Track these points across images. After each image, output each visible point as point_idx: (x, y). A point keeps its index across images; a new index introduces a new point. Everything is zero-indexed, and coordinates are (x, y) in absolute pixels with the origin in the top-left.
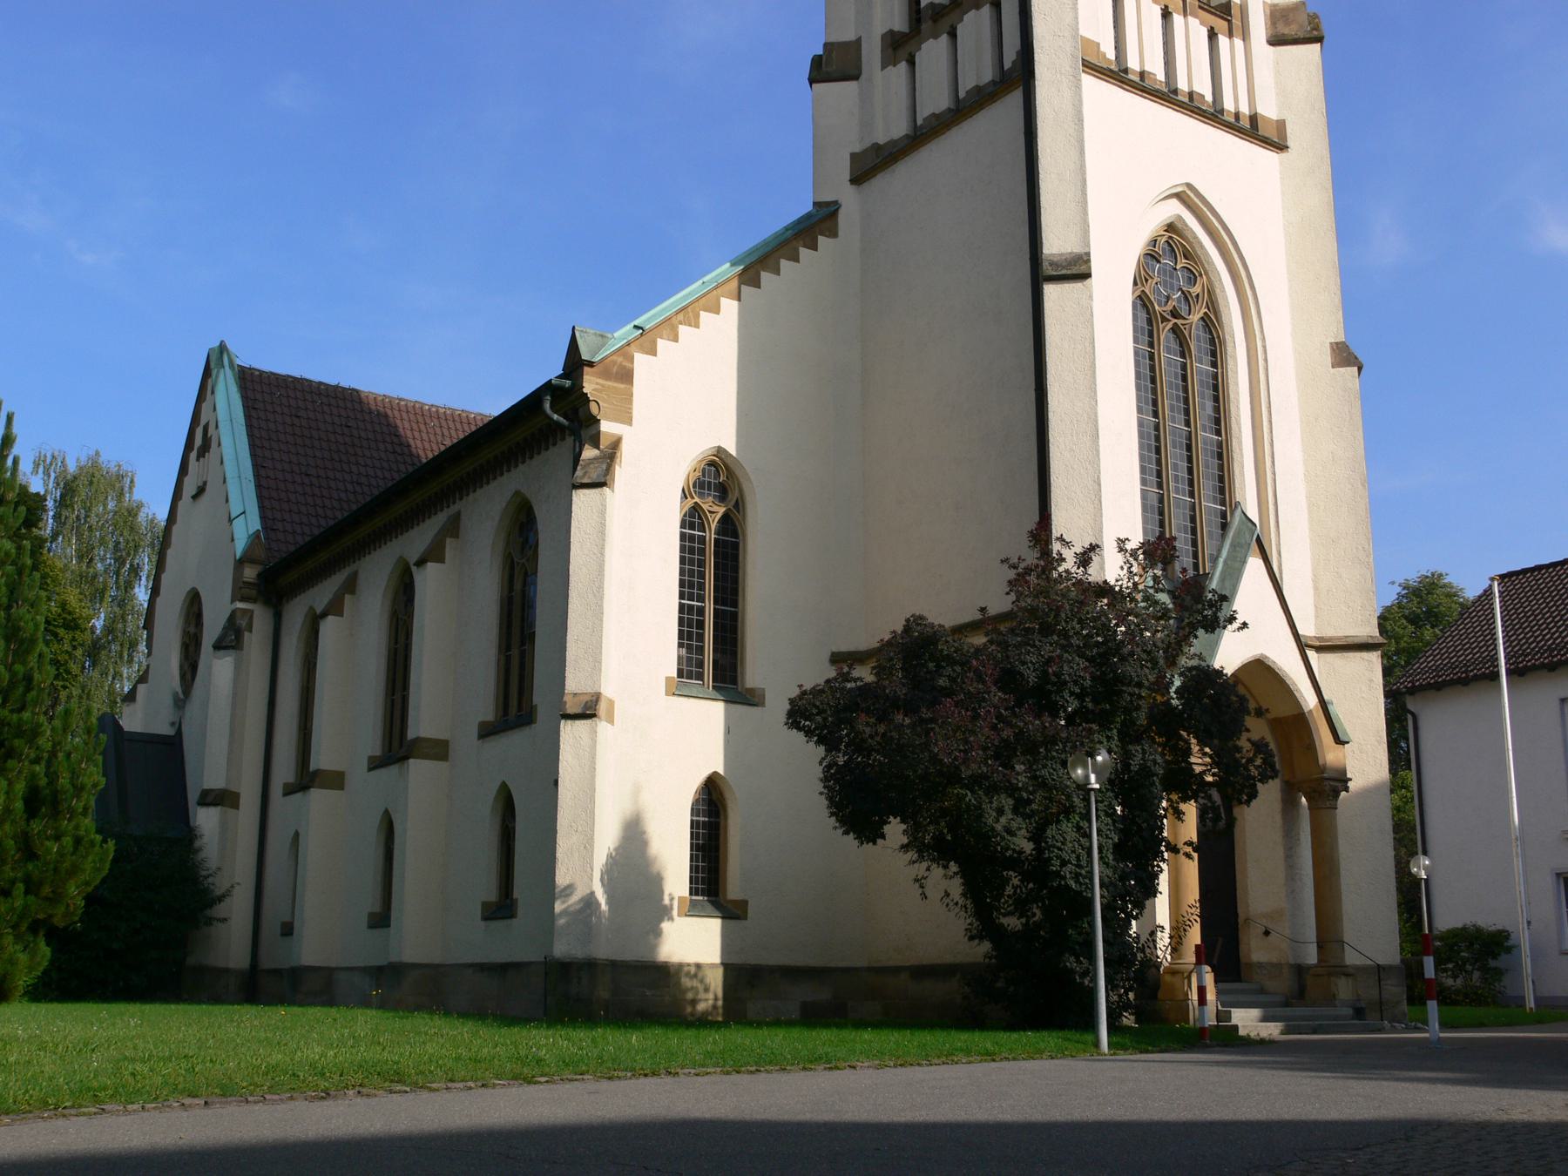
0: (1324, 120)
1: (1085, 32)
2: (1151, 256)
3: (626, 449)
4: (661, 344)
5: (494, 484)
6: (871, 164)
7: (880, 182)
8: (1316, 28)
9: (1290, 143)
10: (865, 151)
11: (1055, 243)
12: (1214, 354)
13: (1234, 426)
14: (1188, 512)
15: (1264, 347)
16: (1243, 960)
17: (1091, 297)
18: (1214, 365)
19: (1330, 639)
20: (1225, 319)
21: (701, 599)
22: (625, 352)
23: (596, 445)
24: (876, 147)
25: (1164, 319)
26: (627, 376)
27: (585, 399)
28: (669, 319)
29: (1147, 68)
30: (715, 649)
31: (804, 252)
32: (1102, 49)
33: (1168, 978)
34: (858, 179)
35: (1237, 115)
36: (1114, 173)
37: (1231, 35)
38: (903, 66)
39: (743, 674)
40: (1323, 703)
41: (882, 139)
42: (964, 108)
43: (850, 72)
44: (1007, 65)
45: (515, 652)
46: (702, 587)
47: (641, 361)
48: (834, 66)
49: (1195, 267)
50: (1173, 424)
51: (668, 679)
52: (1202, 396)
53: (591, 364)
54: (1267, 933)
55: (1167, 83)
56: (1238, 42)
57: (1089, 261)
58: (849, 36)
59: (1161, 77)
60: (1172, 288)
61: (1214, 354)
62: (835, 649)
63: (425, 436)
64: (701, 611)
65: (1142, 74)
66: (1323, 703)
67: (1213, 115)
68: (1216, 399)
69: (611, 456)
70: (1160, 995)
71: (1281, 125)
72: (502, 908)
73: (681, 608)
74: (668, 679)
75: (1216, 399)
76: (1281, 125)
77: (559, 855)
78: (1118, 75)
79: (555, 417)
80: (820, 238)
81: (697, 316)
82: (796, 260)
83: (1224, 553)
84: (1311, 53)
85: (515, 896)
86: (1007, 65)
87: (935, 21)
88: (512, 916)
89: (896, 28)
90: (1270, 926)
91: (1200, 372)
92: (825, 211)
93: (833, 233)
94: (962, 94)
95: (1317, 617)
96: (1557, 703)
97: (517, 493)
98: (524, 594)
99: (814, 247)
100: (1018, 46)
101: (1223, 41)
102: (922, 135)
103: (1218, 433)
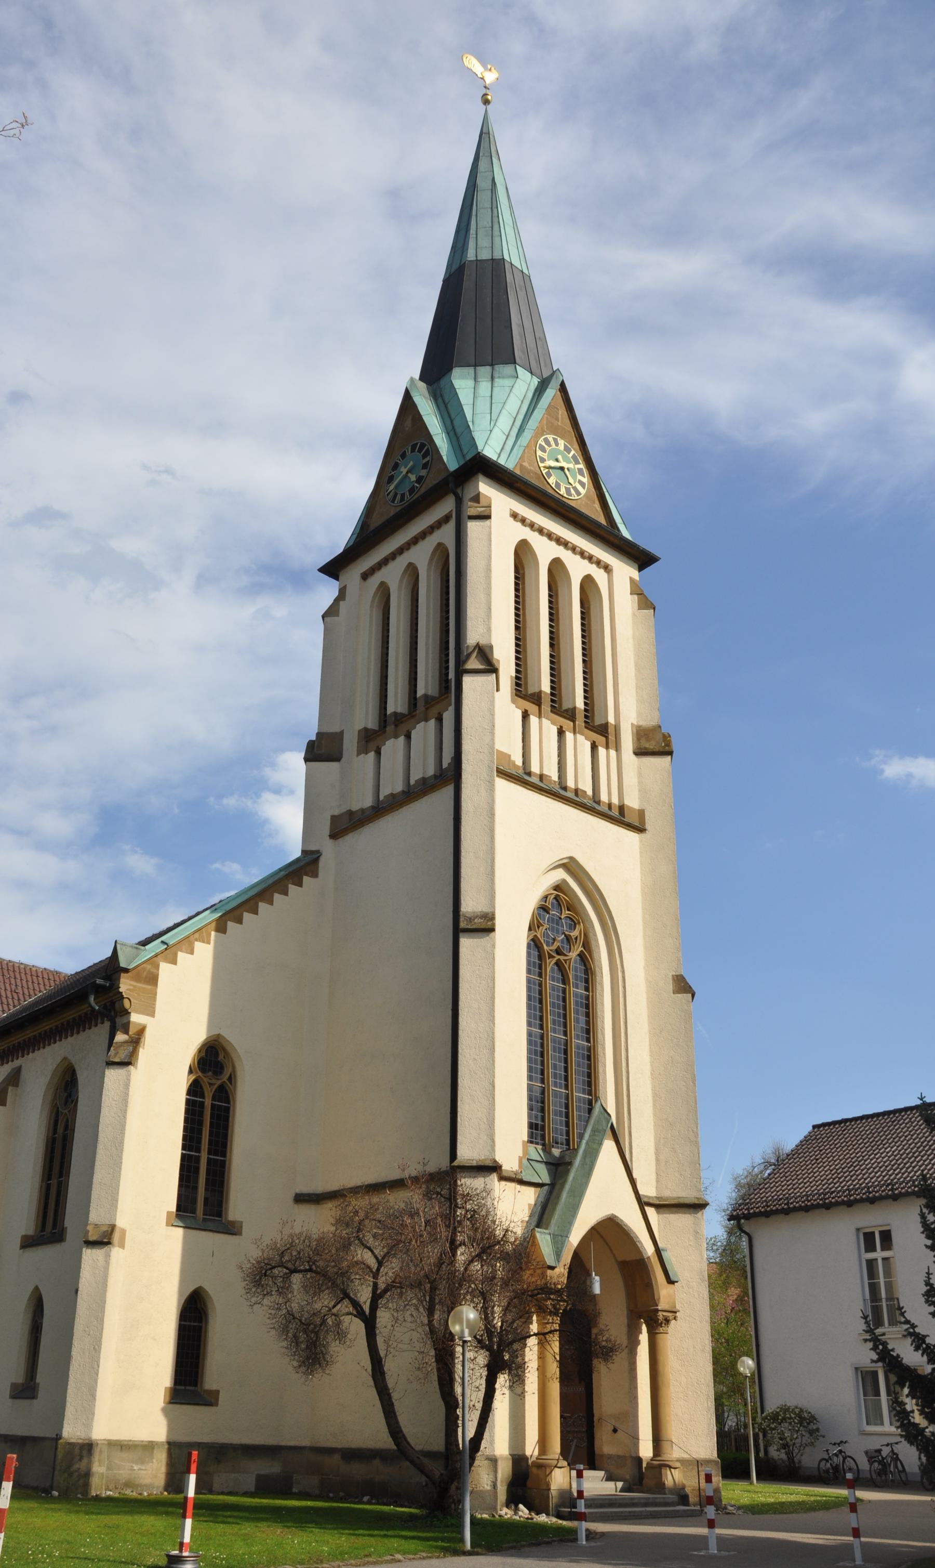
1: (500, 746)
2: (543, 908)
3: (148, 1033)
4: (181, 956)
6: (346, 824)
8: (668, 744)
9: (648, 826)
10: (342, 815)
11: (470, 904)
12: (587, 981)
13: (600, 1036)
14: (563, 1101)
16: (597, 1451)
17: (494, 946)
18: (587, 989)
19: (667, 1199)
20: (595, 955)
21: (198, 1150)
22: (153, 961)
23: (126, 1032)
24: (350, 813)
25: (551, 956)
26: (153, 980)
27: (121, 997)
28: (188, 937)
30: (203, 1194)
32: (513, 758)
33: (534, 1470)
34: (335, 835)
35: (610, 806)
36: (520, 848)
37: (607, 747)
38: (372, 754)
39: (227, 1209)
40: (658, 1251)
41: (355, 807)
42: (412, 794)
43: (335, 757)
44: (445, 765)
45: (54, 1182)
47: (165, 968)
49: (576, 917)
50: (554, 1035)
51: (169, 1213)
52: (577, 1012)
53: (126, 971)
54: (615, 1431)
55: (560, 783)
56: (613, 753)
57: (493, 918)
58: (335, 729)
60: (558, 932)
61: (587, 981)
62: (298, 1191)
64: (198, 1159)
65: (541, 777)
66: (658, 1251)
68: (587, 1015)
69: (136, 1041)
70: (529, 1483)
71: (641, 813)
72: (26, 1390)
73: (183, 1156)
74: (169, 1213)
75: (587, 1015)
76: (641, 813)
77: (74, 1353)
83: (587, 1136)
85: (37, 1381)
86: (445, 765)
87: (396, 726)
88: (33, 1397)
89: (370, 726)
90: (617, 1425)
91: (576, 995)
92: (309, 858)
93: (315, 874)
94: (412, 782)
95: (657, 1181)
96: (854, 1231)
97: (65, 1058)
101: (602, 751)
102: (383, 808)
103: (588, 1040)
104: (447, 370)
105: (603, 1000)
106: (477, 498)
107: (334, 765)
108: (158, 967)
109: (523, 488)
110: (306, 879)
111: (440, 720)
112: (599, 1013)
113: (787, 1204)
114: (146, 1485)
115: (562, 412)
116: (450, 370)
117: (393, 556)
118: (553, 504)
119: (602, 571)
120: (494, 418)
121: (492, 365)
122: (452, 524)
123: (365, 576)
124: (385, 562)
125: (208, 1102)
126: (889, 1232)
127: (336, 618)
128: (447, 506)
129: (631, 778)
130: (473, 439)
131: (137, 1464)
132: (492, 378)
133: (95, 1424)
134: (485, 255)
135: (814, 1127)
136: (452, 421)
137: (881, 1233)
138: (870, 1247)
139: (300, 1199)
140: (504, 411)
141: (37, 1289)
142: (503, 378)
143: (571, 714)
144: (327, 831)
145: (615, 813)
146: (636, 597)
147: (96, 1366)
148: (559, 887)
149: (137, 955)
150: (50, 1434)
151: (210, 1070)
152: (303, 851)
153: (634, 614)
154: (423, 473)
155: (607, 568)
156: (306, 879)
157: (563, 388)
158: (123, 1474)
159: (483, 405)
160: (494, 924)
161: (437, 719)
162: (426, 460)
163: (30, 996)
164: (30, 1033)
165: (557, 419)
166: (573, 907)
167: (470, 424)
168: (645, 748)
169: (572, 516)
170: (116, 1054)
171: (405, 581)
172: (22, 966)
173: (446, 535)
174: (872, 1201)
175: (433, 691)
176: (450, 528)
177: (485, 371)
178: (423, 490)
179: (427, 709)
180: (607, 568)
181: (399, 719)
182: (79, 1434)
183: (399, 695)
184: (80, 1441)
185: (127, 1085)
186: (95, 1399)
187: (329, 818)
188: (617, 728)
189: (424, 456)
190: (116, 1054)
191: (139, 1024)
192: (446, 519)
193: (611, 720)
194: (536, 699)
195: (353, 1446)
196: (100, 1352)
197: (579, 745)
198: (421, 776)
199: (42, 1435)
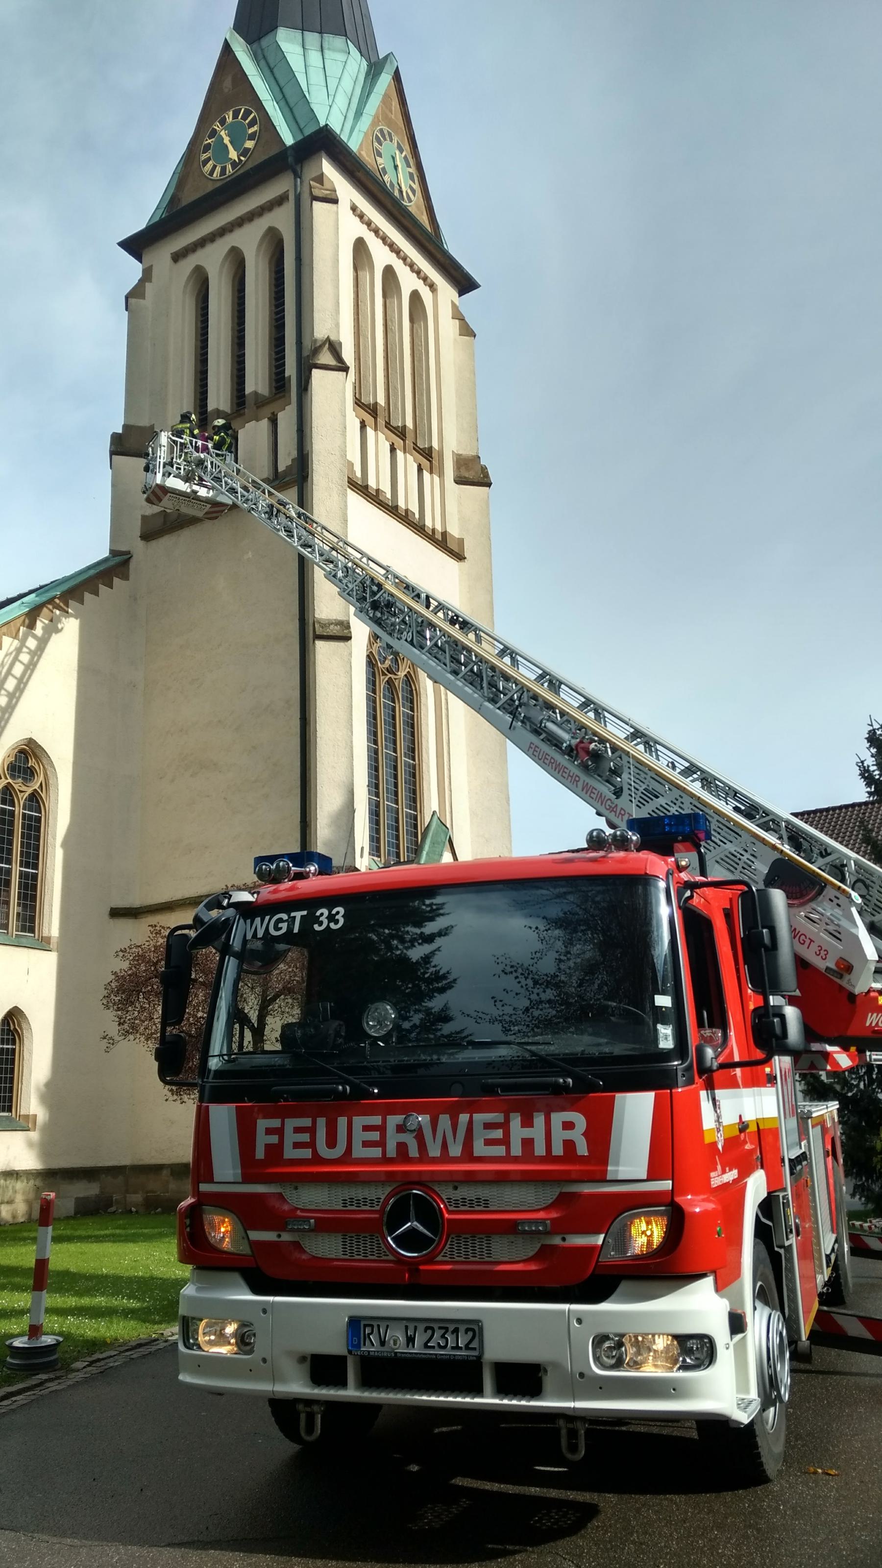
7: (165, 542)
8: (486, 475)
31: (102, 588)
34: (148, 536)
35: (433, 530)
37: (431, 472)
50: (384, 751)
56: (436, 479)
62: (114, 905)
67: (419, 528)
71: (461, 542)
76: (461, 542)
78: (362, 488)
82: (97, 594)
92: (118, 559)
100: (294, 454)
101: (426, 475)
106: (320, 179)
110: (116, 581)
111: (274, 421)
117: (212, 238)
118: (389, 206)
119: (428, 288)
120: (331, 92)
121: (321, 33)
132: (322, 51)
136: (281, 89)
139: (116, 913)
140: (340, 87)
146: (457, 321)
151: (19, 777)
153: (455, 340)
155: (432, 287)
157: (397, 77)
159: (316, 77)
165: (391, 111)
168: (465, 477)
171: (264, 245)
173: (282, 220)
176: (288, 209)
177: (312, 38)
178: (249, 166)
180: (432, 287)
181: (261, 402)
183: (221, 393)
187: (140, 517)
192: (280, 201)
193: (435, 445)
197: (407, 463)
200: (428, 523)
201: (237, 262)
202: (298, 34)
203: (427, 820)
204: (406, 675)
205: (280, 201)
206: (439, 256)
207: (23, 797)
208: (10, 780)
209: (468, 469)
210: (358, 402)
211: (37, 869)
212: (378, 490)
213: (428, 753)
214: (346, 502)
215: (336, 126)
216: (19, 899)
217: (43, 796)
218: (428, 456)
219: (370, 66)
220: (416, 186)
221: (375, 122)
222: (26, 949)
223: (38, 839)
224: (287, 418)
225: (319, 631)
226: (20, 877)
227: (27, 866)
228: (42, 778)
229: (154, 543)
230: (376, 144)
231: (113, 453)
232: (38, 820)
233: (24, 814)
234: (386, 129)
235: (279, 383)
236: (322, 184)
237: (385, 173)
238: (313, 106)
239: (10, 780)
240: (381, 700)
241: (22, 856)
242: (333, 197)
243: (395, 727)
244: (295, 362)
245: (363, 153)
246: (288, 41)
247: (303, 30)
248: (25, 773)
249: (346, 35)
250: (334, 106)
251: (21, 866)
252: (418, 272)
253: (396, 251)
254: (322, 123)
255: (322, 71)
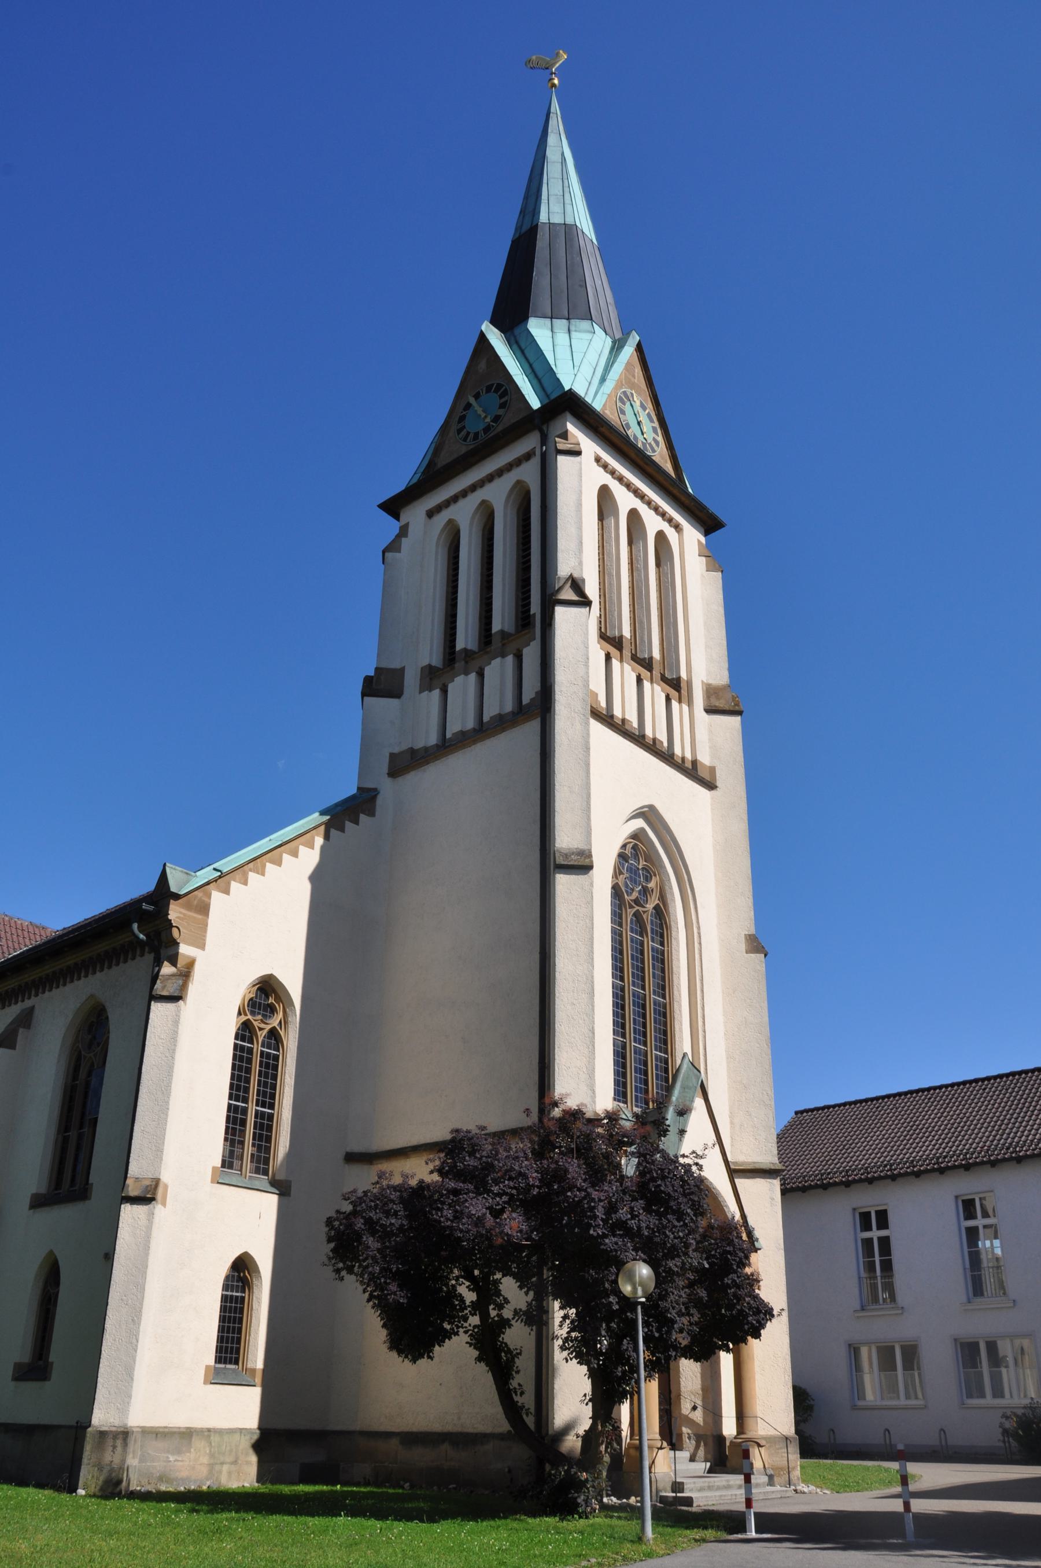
0: (743, 770)
4: (234, 886)
5: (69, 987)
6: (407, 762)
7: (412, 778)
8: (737, 705)
9: (718, 784)
11: (565, 839)
13: (676, 993)
15: (699, 934)
17: (592, 884)
19: (743, 1163)
20: (671, 910)
21: (245, 1100)
23: (174, 962)
24: (412, 752)
25: (631, 907)
26: (204, 909)
27: (169, 925)
29: (627, 717)
30: (245, 1140)
31: (349, 825)
35: (683, 759)
36: (605, 791)
37: (680, 701)
38: (436, 693)
41: (419, 744)
44: (526, 700)
45: (73, 1134)
46: (247, 1090)
48: (381, 685)
49: (652, 868)
53: (177, 897)
56: (685, 707)
57: (590, 856)
58: (395, 665)
59: (635, 725)
61: (662, 936)
62: (349, 1150)
63: (10, 943)
64: (245, 1111)
67: (667, 757)
69: (186, 975)
71: (712, 770)
72: (35, 1369)
74: (214, 1169)
76: (712, 770)
77: (108, 1325)
78: (607, 719)
79: (141, 936)
80: (362, 816)
81: (264, 867)
84: (734, 722)
87: (467, 662)
93: (371, 813)
98: (88, 1084)
99: (356, 822)
100: (538, 687)
101: (675, 704)
102: (447, 746)
104: (523, 318)
105: (678, 955)
106: (565, 435)
107: (394, 702)
108: (209, 896)
109: (607, 433)
110: (363, 817)
111: (519, 657)
112: (675, 969)
113: (938, 1163)
114: (182, 1479)
115: (638, 371)
116: (525, 319)
117: (464, 494)
118: (633, 455)
121: (568, 319)
122: (536, 461)
123: (431, 514)
124: (455, 499)
125: (257, 1048)
126: (885, 1212)
127: (397, 555)
128: (530, 442)
129: (702, 735)
130: (558, 380)
131: (173, 1454)
132: (569, 331)
133: (131, 1409)
134: (557, 219)
135: (796, 1113)
137: (877, 1212)
138: (866, 1226)
141: (51, 1253)
142: (580, 331)
143: (647, 664)
144: (385, 769)
145: (689, 765)
147: (134, 1341)
148: (637, 836)
149: (188, 882)
150: (66, 1419)
151: (259, 1014)
152: (359, 789)
153: (702, 575)
154: (501, 412)
156: (363, 817)
158: (157, 1467)
159: (563, 352)
160: (592, 862)
161: (515, 655)
162: (503, 400)
163: (15, 950)
164: (47, 969)
165: (634, 376)
166: (651, 857)
167: (553, 367)
169: (650, 470)
170: (164, 988)
172: (7, 919)
173: (529, 473)
174: (870, 1181)
175: (510, 627)
177: (561, 324)
178: (500, 428)
179: (503, 645)
180: (677, 527)
182: (112, 1420)
184: (114, 1429)
185: (176, 1022)
186: (132, 1379)
187: (388, 755)
188: (689, 683)
189: (501, 397)
190: (164, 988)
191: (188, 957)
192: (528, 456)
193: (684, 675)
194: (617, 643)
195: (415, 1430)
196: (139, 1324)
197: (655, 693)
198: (497, 712)
199: (55, 1422)
200: (678, 751)
201: (487, 516)
202: (548, 321)
203: (678, 1062)
204: (654, 908)
205: (528, 456)
206: (683, 499)
207: (261, 1035)
208: (249, 1017)
209: (718, 698)
210: (603, 636)
211: (273, 1109)
212: (623, 720)
213: (679, 991)
214: (588, 730)
215: (580, 390)
216: (254, 1139)
217: (282, 1033)
218: (675, 685)
219: (614, 342)
220: (660, 439)
221: (619, 384)
222: (259, 1193)
223: (275, 1077)
224: (531, 654)
225: (560, 860)
226: (256, 1117)
227: (263, 1106)
228: (281, 1015)
229: (400, 779)
230: (619, 404)
231: (364, 695)
232: (276, 1058)
233: (262, 1052)
234: (629, 391)
235: (524, 619)
236: (566, 439)
237: (629, 427)
238: (558, 376)
239: (249, 1017)
240: (628, 934)
241: (258, 1095)
242: (576, 449)
243: (643, 962)
244: (536, 596)
245: (607, 412)
246: (538, 329)
247: (552, 318)
248: (265, 1010)
249: (591, 319)
250: (579, 375)
251: (257, 1105)
252: (663, 515)
253: (637, 493)
254: (567, 388)
255: (569, 349)
